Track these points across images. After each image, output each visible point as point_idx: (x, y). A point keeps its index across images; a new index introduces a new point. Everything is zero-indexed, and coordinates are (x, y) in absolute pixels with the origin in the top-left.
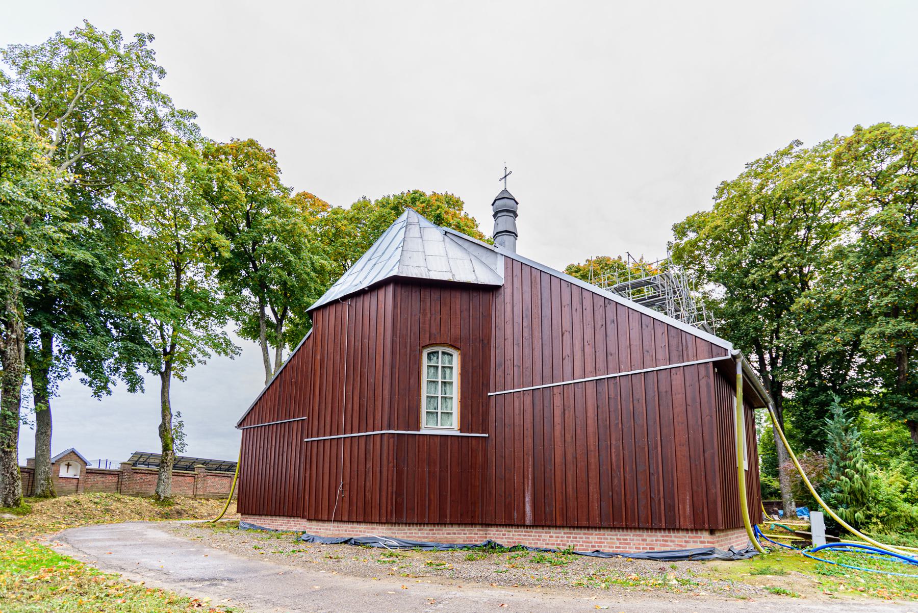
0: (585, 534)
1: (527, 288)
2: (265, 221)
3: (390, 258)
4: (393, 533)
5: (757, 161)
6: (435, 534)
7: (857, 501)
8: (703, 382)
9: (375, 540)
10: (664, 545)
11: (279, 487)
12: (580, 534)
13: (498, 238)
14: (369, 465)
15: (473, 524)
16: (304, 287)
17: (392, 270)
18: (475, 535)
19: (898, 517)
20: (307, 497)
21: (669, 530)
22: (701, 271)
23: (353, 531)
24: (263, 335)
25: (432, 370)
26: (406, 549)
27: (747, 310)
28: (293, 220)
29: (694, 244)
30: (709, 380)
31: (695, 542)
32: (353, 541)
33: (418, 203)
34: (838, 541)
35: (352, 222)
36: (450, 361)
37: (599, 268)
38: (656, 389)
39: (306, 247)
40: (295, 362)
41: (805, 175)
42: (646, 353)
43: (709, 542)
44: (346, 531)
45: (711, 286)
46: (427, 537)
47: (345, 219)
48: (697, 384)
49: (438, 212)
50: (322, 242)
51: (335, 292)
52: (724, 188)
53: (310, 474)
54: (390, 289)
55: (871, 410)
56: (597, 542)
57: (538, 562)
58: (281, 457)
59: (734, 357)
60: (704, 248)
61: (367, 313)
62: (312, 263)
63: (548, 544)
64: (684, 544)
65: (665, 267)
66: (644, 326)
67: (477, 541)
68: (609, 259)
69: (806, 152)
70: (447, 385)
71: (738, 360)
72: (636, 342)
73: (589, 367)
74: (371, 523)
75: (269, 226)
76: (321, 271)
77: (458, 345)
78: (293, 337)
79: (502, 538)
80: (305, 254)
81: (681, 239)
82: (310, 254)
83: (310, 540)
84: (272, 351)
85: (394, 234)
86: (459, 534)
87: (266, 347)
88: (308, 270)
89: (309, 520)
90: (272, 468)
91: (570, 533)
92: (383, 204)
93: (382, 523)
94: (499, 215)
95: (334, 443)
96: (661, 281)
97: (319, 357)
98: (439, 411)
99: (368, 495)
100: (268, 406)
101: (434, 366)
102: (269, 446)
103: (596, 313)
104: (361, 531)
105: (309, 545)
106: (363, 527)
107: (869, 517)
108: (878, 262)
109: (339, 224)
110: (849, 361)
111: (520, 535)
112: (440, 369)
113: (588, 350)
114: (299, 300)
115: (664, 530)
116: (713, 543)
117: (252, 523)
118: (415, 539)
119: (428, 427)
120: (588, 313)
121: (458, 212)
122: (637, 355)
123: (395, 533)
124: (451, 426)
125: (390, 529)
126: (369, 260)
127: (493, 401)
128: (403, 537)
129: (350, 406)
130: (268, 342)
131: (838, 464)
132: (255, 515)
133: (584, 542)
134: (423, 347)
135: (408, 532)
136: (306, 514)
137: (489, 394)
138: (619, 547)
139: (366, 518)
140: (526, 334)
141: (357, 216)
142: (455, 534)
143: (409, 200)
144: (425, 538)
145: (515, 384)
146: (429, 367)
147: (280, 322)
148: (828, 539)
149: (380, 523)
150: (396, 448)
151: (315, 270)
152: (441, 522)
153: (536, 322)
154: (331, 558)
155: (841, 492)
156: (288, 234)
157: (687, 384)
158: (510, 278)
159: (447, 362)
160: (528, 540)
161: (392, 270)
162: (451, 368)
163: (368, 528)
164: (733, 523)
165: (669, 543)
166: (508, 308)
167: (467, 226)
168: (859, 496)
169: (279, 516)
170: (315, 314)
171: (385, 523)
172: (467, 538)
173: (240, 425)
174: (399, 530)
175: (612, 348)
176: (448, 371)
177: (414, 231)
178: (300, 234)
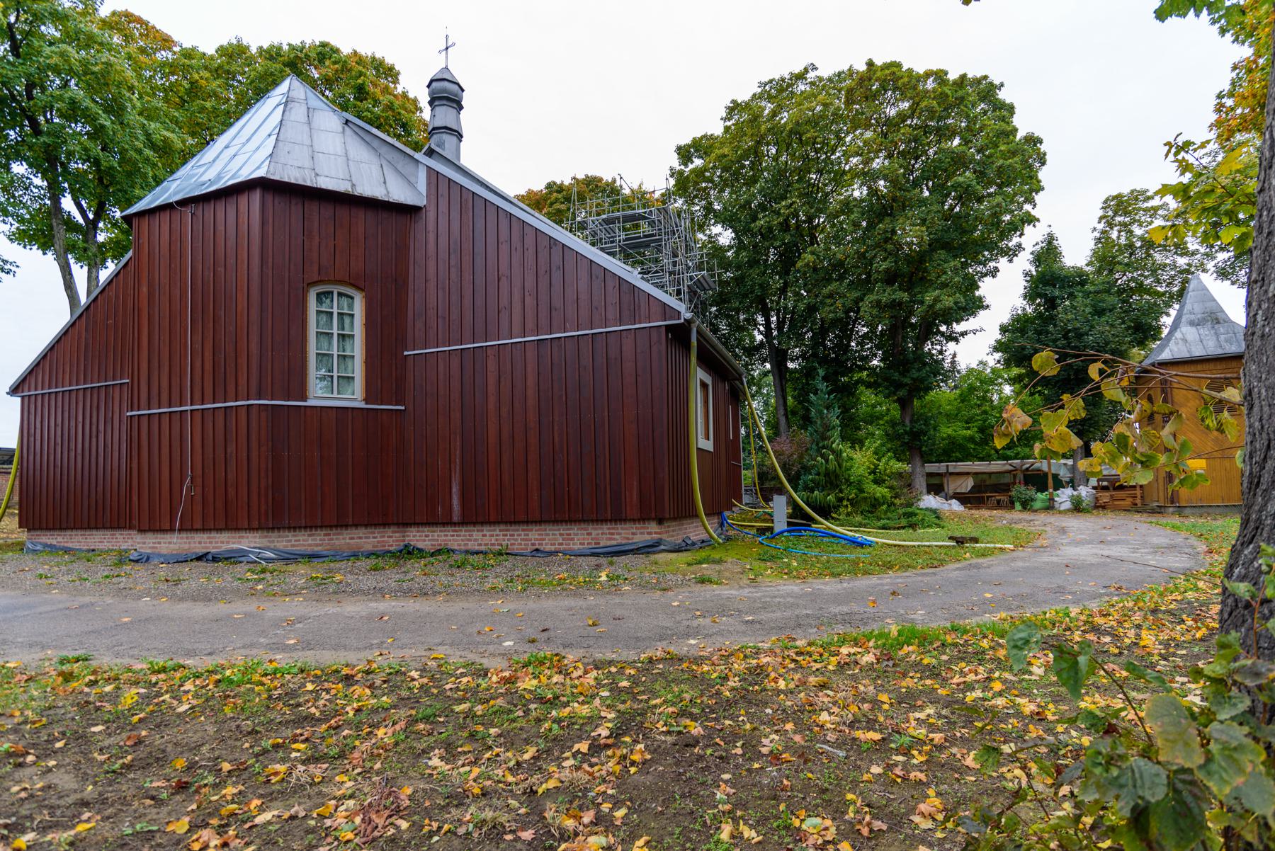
0: (523, 530)
1: (455, 215)
2: (47, 50)
3: (258, 148)
4: (270, 542)
5: (771, 81)
6: (332, 539)
7: (831, 483)
8: (654, 348)
9: (243, 553)
10: (611, 539)
11: (93, 485)
12: (518, 530)
13: (435, 136)
14: (231, 448)
15: (385, 525)
16: (133, 172)
17: (258, 168)
18: (390, 539)
19: (865, 499)
20: (135, 498)
21: (616, 521)
22: (708, 209)
23: (211, 543)
24: (59, 243)
25: (324, 318)
26: (289, 562)
27: (753, 263)
28: (106, 56)
29: (699, 173)
30: (661, 345)
31: (641, 533)
32: (210, 557)
33: (327, 63)
34: (810, 526)
35: (219, 76)
36: (351, 307)
37: (587, 190)
38: (605, 355)
39: (134, 107)
40: (112, 294)
41: (819, 108)
42: (594, 310)
43: (656, 533)
44: (200, 543)
45: (717, 229)
46: (320, 545)
47: (206, 68)
48: (648, 351)
49: (360, 81)
50: (166, 100)
51: (174, 189)
52: (734, 108)
53: (139, 463)
54: (257, 196)
55: (869, 386)
56: (537, 540)
57: (458, 567)
58: (94, 440)
59: (688, 322)
60: (712, 181)
61: (221, 228)
62: (148, 135)
63: (481, 545)
64: (631, 536)
65: (667, 197)
66: (594, 277)
67: (392, 546)
68: (601, 180)
69: (821, 79)
70: (347, 339)
71: (693, 325)
72: (584, 296)
73: (530, 324)
74: (237, 529)
75: (55, 60)
76: (164, 149)
77: (362, 284)
78: (116, 249)
79: (425, 541)
80: (132, 117)
81: (686, 166)
82: (142, 120)
83: (143, 560)
84: (80, 274)
85: (266, 112)
86: (366, 538)
87: (68, 265)
88: (139, 144)
89: (141, 531)
90: (79, 458)
91: (507, 530)
92: (272, 54)
93: (253, 529)
94: (436, 103)
95: (176, 418)
96: (658, 216)
97: (145, 289)
98: (335, 374)
99: (231, 491)
100: (68, 360)
101: (326, 312)
102: (73, 424)
103: (539, 255)
104: (222, 542)
105: (138, 567)
106: (225, 536)
107: (841, 500)
108: (880, 222)
109: (196, 77)
110: (852, 330)
111: (447, 535)
112: (335, 316)
113: (529, 301)
114: (126, 192)
115: (611, 521)
116: (659, 533)
117: (49, 542)
118: (303, 548)
119: (319, 394)
120: (530, 254)
121: (392, 85)
122: (585, 313)
123: (273, 542)
124: (354, 396)
125: (266, 537)
126: (227, 147)
127: (410, 362)
128: (287, 546)
129: (198, 364)
130: (70, 256)
131: (817, 445)
132: (54, 529)
133: (522, 540)
134: (308, 285)
135: (293, 539)
136: (135, 522)
137: (406, 353)
138: (561, 544)
139: (230, 524)
140: (453, 276)
141: (227, 67)
142: (361, 538)
143: (313, 55)
144: (317, 545)
145: (440, 341)
146: (319, 312)
147: (92, 226)
148: (789, 524)
149: (250, 529)
150: (270, 424)
151: (153, 146)
152: (341, 524)
153: (467, 259)
154: (167, 581)
155: (818, 474)
156: (98, 80)
157: (638, 351)
158: (433, 197)
159: (346, 306)
160: (457, 541)
161: (258, 168)
162: (352, 316)
163: (233, 537)
164: (686, 512)
165: (616, 536)
166: (431, 237)
167: (405, 109)
168: (833, 478)
169: (97, 528)
170: (135, 222)
171: (257, 529)
172: (378, 542)
173: (14, 391)
174: (279, 537)
175: (557, 303)
176: (347, 320)
177: (298, 112)
178: (120, 83)
